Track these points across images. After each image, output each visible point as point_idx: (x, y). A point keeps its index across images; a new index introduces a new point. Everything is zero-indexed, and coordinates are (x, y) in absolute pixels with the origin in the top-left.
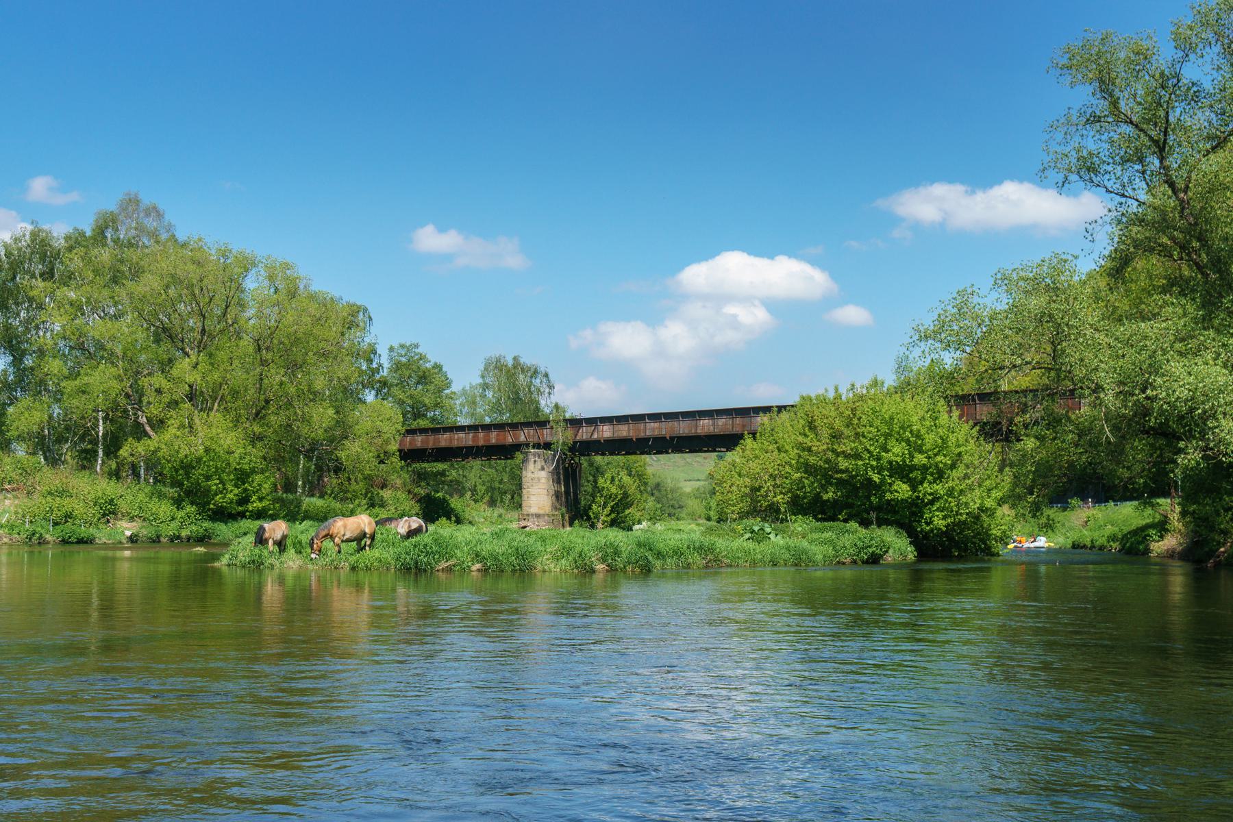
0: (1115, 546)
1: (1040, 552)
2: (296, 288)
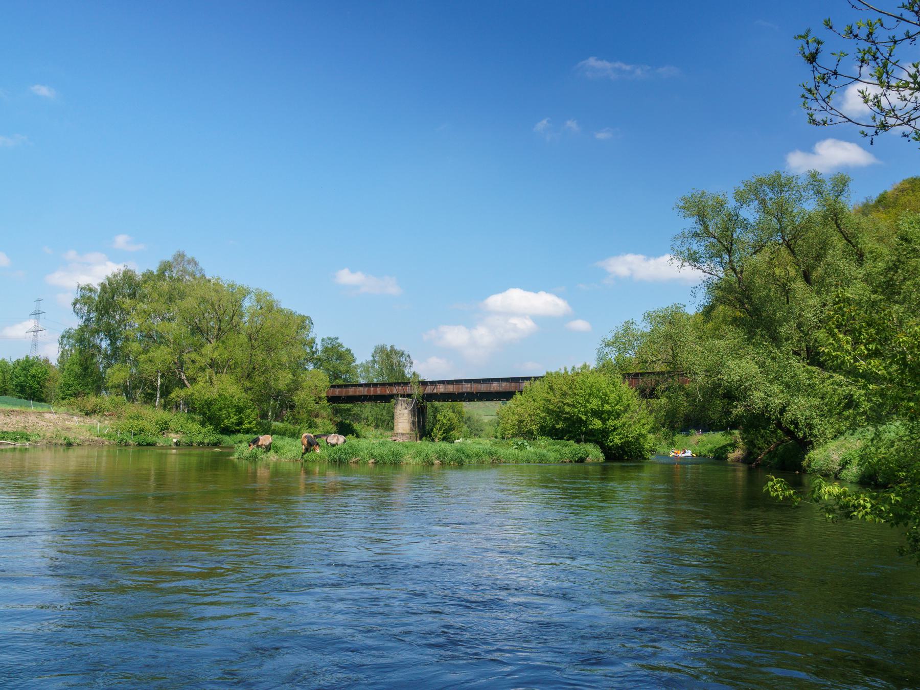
0: (712, 455)
1: (688, 459)
2: (272, 306)
